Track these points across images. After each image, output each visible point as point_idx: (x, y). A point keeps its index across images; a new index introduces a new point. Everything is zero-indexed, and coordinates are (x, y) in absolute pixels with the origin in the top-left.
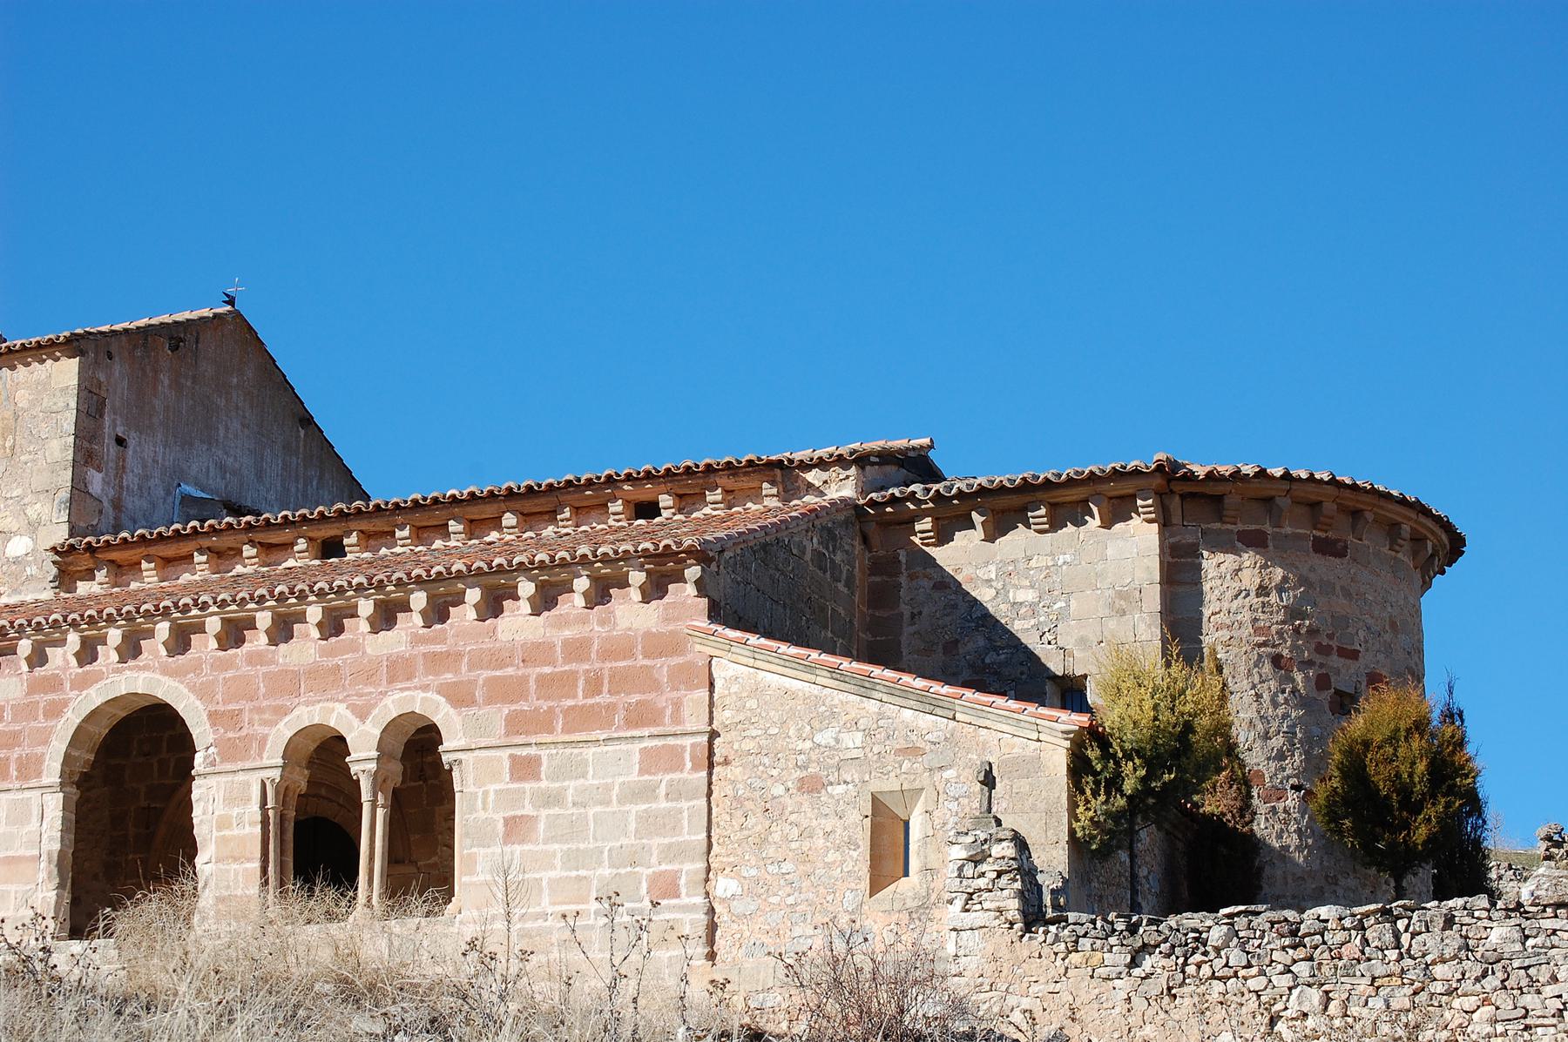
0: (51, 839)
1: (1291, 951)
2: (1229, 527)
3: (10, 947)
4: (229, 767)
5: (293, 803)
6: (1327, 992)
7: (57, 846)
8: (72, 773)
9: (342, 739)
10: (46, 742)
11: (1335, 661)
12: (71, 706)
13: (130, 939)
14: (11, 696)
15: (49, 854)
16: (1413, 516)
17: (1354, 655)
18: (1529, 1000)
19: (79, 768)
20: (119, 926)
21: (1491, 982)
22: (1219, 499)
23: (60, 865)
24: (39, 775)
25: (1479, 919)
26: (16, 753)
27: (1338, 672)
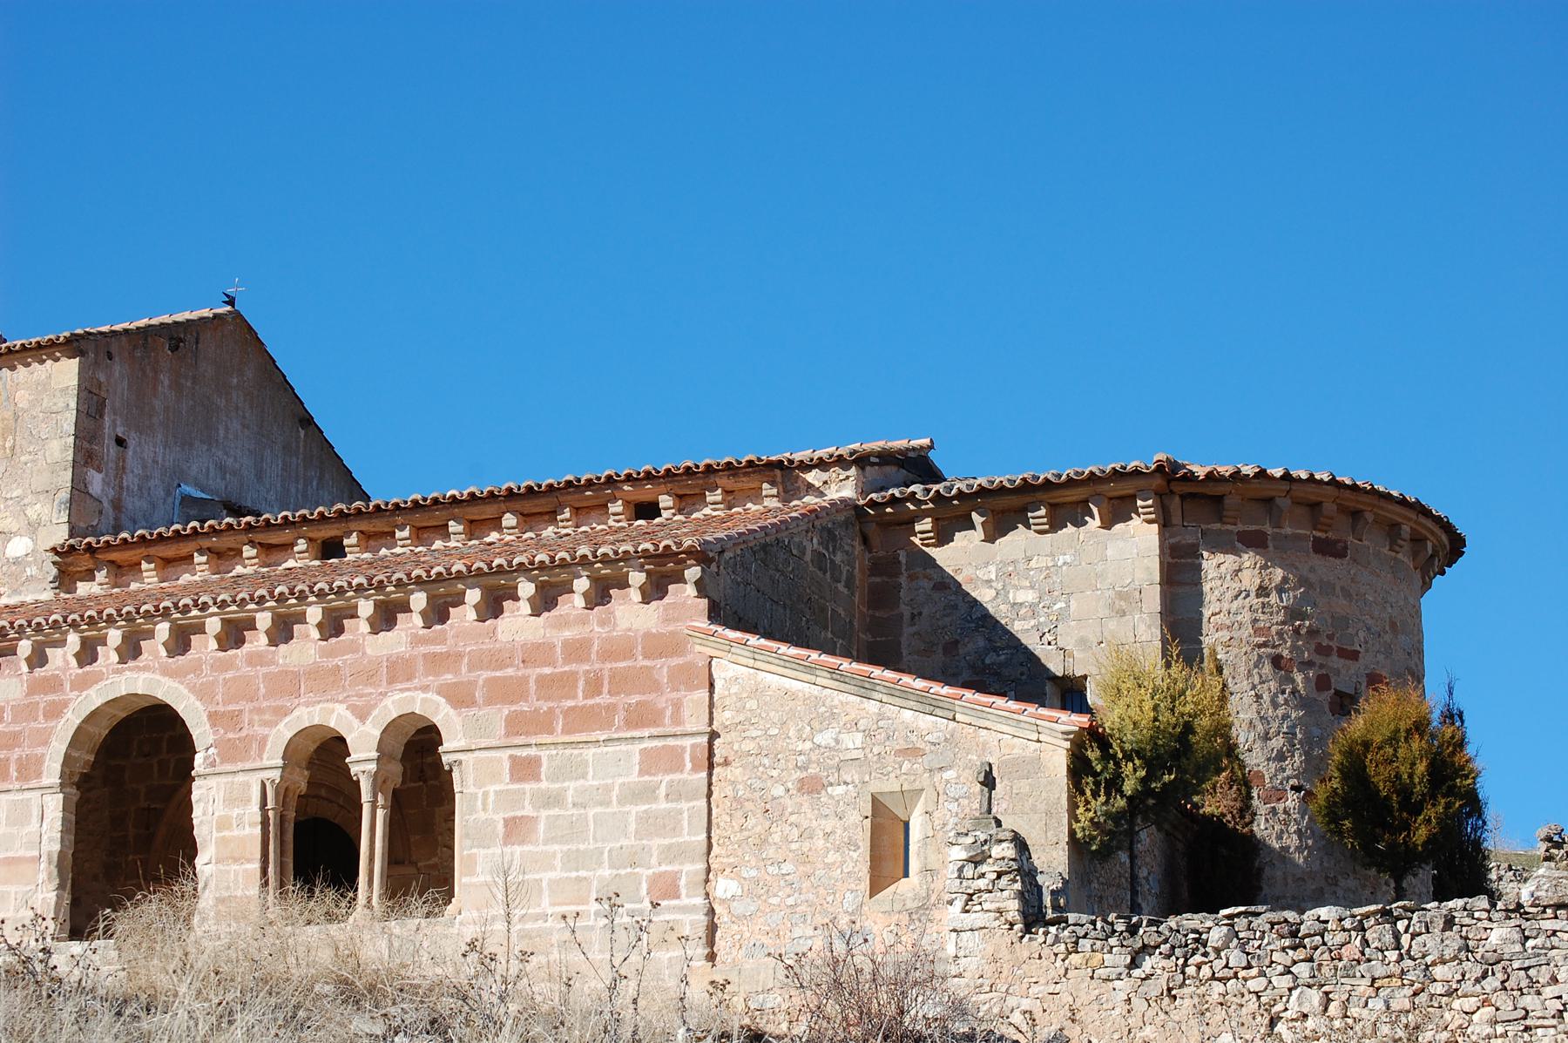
0: (51, 840)
1: (1291, 952)
2: (1229, 527)
3: (10, 948)
4: (229, 767)
5: (293, 804)
6: (1327, 993)
7: (57, 847)
8: (72, 774)
9: (342, 740)
10: (46, 743)
11: (1335, 662)
12: (71, 706)
13: (130, 941)
14: (11, 696)
15: (49, 855)
16: (1413, 516)
17: (1354, 656)
18: (1529, 1001)
19: (79, 768)
20: (119, 927)
21: (1491, 983)
22: (1219, 499)
23: (60, 866)
24: (39, 775)
25: (1479, 920)
26: (16, 753)
27: (1338, 672)
